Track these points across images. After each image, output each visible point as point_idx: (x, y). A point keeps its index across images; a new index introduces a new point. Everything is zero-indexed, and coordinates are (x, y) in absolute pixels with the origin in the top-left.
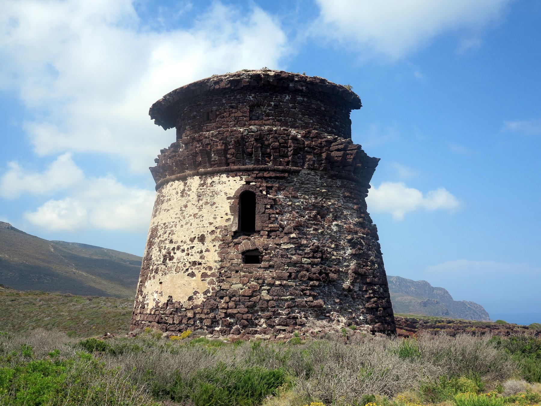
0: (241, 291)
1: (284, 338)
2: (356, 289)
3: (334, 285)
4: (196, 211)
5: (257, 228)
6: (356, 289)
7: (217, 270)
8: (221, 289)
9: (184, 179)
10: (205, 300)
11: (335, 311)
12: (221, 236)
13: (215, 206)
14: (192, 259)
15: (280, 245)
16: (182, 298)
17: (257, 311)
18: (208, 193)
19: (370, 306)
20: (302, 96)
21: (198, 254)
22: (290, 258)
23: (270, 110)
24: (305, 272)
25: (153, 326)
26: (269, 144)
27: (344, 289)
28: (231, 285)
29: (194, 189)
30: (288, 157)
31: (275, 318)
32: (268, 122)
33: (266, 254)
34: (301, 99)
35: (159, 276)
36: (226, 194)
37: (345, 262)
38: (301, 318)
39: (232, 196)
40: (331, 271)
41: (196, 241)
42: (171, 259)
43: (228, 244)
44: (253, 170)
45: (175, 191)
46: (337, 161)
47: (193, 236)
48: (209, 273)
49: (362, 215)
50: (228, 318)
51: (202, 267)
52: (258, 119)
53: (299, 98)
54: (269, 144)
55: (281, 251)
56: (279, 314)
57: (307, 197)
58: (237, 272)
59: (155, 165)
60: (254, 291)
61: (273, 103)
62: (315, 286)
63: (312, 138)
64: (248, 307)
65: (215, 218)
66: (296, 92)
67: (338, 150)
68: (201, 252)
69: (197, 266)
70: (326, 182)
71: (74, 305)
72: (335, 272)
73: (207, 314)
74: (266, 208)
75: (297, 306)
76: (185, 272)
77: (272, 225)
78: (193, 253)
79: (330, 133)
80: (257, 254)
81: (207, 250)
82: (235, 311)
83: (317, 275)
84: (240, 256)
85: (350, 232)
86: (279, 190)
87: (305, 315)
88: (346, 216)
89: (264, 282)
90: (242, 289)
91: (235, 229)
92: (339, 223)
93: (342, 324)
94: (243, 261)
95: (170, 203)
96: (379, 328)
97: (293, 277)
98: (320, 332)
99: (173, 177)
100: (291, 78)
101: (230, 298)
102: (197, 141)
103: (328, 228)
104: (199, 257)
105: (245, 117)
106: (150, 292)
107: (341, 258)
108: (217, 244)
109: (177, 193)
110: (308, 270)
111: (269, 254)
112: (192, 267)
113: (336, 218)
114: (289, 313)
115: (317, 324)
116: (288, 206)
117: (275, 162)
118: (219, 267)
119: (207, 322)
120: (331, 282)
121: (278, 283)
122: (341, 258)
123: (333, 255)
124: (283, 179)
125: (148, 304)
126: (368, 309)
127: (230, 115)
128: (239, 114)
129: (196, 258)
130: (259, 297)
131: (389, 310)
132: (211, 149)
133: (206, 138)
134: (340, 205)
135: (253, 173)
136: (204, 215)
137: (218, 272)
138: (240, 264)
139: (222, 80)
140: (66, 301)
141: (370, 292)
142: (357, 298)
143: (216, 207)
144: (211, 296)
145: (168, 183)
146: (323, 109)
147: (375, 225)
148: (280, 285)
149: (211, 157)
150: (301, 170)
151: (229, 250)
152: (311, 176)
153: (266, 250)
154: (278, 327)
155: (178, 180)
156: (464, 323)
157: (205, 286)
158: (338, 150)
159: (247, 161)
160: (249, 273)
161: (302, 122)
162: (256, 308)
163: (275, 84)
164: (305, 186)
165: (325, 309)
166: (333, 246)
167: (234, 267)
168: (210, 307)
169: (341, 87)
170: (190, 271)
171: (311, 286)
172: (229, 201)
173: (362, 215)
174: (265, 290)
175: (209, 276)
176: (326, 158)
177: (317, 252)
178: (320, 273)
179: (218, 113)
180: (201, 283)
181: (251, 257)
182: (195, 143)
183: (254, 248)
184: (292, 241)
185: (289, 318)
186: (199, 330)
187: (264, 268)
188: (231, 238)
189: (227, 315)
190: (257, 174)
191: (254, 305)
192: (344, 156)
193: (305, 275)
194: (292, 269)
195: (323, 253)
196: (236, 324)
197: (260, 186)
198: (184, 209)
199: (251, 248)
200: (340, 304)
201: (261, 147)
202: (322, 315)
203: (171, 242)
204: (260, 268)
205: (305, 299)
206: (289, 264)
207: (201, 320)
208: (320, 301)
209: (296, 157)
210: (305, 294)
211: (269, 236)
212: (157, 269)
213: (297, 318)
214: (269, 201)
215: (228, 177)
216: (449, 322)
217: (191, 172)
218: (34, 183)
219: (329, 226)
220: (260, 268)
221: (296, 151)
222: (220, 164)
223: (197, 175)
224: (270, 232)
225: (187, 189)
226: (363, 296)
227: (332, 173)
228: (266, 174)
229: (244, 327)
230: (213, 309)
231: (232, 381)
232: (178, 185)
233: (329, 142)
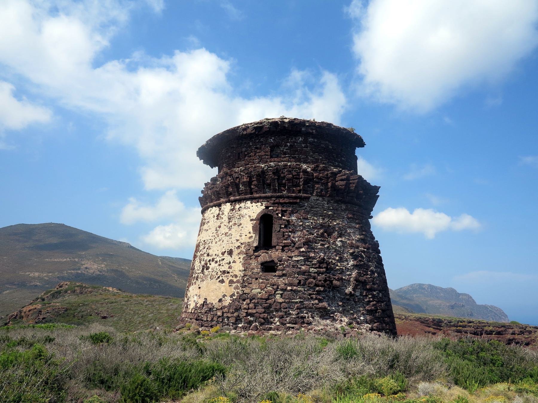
0: (259, 295)
1: (292, 334)
2: (358, 294)
3: (338, 291)
4: (227, 230)
5: (273, 244)
6: (358, 294)
8: (243, 293)
9: (219, 205)
11: (338, 312)
13: (241, 226)
14: (223, 269)
15: (292, 257)
17: (272, 312)
19: (369, 309)
20: (312, 138)
22: (300, 268)
23: (286, 149)
24: (312, 280)
25: (192, 323)
26: (285, 177)
27: (346, 294)
29: (226, 213)
30: (300, 186)
31: (287, 317)
32: (285, 159)
33: (280, 265)
35: (198, 282)
36: (250, 216)
37: (348, 271)
38: (308, 317)
39: (254, 218)
40: (335, 278)
41: (226, 254)
42: (208, 268)
43: (251, 256)
45: (212, 215)
46: (341, 189)
47: (224, 251)
48: (235, 280)
49: (364, 233)
52: (277, 157)
53: (311, 140)
54: (285, 177)
56: (290, 314)
57: (316, 218)
58: (257, 279)
59: (202, 195)
60: (270, 295)
61: (289, 144)
62: (320, 291)
63: (320, 171)
64: (264, 308)
65: (241, 236)
66: (307, 135)
67: (342, 180)
68: (230, 263)
69: (226, 275)
70: (332, 206)
71: (171, 305)
72: (338, 280)
73: (233, 313)
74: (281, 228)
75: (305, 308)
76: (217, 279)
77: (286, 242)
79: (336, 167)
80: (273, 265)
81: (234, 262)
82: (254, 311)
84: (260, 266)
85: (352, 246)
86: (292, 213)
87: (311, 315)
88: (349, 233)
89: (278, 288)
90: (260, 293)
91: (256, 244)
92: (343, 239)
93: (344, 324)
94: (263, 270)
95: (209, 224)
96: (377, 327)
97: (302, 283)
98: (322, 329)
99: (212, 204)
101: (251, 300)
102: (230, 175)
103: (333, 244)
105: (267, 155)
106: (192, 295)
107: (344, 268)
108: (242, 256)
109: (214, 216)
110: (314, 278)
111: (283, 264)
113: (340, 235)
114: (298, 314)
115: (322, 323)
116: (301, 226)
117: (289, 190)
118: (242, 275)
119: (232, 320)
120: (335, 288)
121: (289, 288)
122: (344, 268)
123: (337, 266)
124: (295, 204)
125: (190, 305)
126: (368, 311)
127: (255, 155)
128: (262, 153)
129: (226, 268)
130: (273, 300)
131: (388, 312)
132: (239, 182)
133: (236, 173)
134: (344, 224)
136: (233, 233)
139: (248, 127)
140: (166, 302)
141: (370, 296)
142: (358, 301)
145: (208, 209)
146: (331, 147)
147: (377, 241)
148: (291, 290)
149: (240, 188)
150: (310, 197)
151: (251, 262)
153: (280, 261)
154: (288, 325)
155: (215, 206)
156: (483, 323)
157: (232, 290)
158: (342, 180)
159: (267, 190)
160: (267, 280)
162: (271, 309)
163: (290, 129)
164: (315, 209)
166: (337, 258)
168: (234, 307)
169: (344, 129)
170: (221, 278)
171: (317, 291)
173: (364, 233)
174: (279, 294)
175: (235, 283)
176: (331, 187)
177: (323, 263)
178: (325, 280)
179: (246, 153)
180: (229, 288)
181: (269, 267)
182: (228, 177)
183: (271, 259)
184: (302, 254)
185: (298, 317)
186: (226, 326)
187: (278, 276)
189: (248, 314)
191: (270, 306)
192: (347, 185)
193: (312, 282)
194: (301, 277)
195: (328, 264)
196: (256, 322)
197: (276, 211)
198: (218, 229)
199: (268, 259)
200: (343, 306)
201: (278, 179)
203: (208, 255)
204: (275, 276)
205: (312, 302)
207: (228, 318)
208: (325, 304)
209: (306, 186)
210: (312, 298)
211: (283, 250)
212: (198, 277)
213: (305, 317)
214: (284, 222)
215: (252, 203)
216: (470, 322)
217: (224, 200)
218: (146, 213)
219: (334, 242)
220: (275, 276)
221: (306, 182)
222: (246, 194)
223: (229, 202)
224: (283, 247)
225: (221, 213)
226: (364, 300)
227: (337, 198)
228: (281, 201)
229: (262, 324)
230: (237, 309)
231: (165, 374)
232: (215, 210)
233: (334, 174)
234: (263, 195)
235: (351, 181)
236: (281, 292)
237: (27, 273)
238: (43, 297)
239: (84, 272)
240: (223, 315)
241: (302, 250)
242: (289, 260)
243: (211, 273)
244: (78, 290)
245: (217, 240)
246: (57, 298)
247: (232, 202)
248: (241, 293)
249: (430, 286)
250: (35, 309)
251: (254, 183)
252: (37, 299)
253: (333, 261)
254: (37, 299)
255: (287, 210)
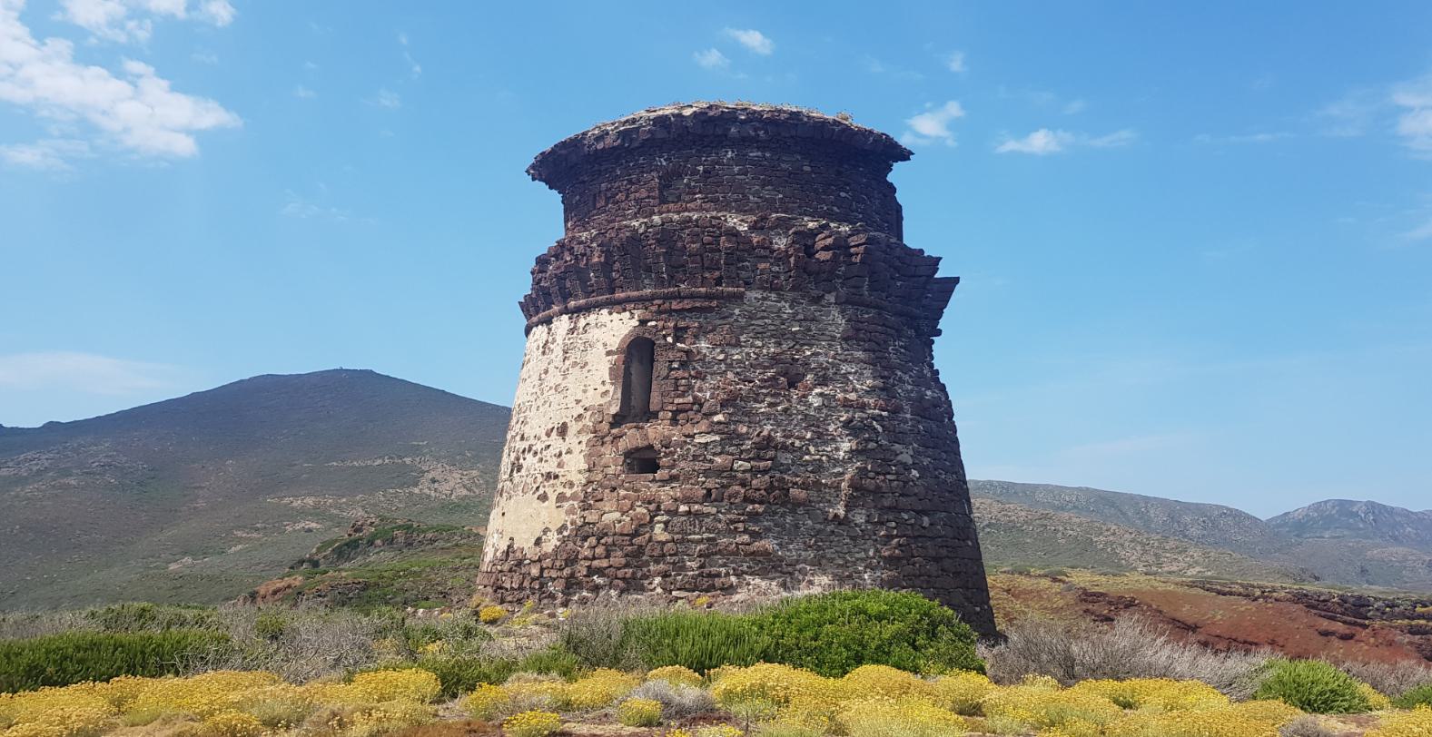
2: (860, 519)
6: (860, 519)
7: (580, 488)
10: (558, 544)
12: (591, 424)
13: (587, 368)
14: (546, 468)
15: (693, 437)
16: (527, 540)
17: (647, 564)
18: (578, 345)
20: (758, 149)
21: (554, 459)
22: (711, 461)
24: (737, 488)
28: (602, 515)
29: (559, 340)
33: (666, 455)
34: (759, 154)
37: (835, 466)
39: (614, 349)
42: (519, 468)
43: (603, 438)
44: (652, 298)
45: (535, 345)
47: (550, 426)
48: (568, 493)
50: (595, 578)
51: (559, 483)
55: (693, 449)
58: (614, 489)
60: (641, 526)
61: (701, 168)
62: (757, 513)
65: (585, 391)
68: (560, 454)
72: (805, 486)
76: (534, 493)
77: (681, 400)
78: (548, 458)
80: (652, 455)
81: (569, 452)
82: (604, 563)
83: (762, 492)
86: (701, 333)
88: (845, 376)
89: (658, 508)
91: (614, 409)
92: (826, 390)
97: (713, 496)
100: (730, 117)
101: (598, 540)
104: (556, 464)
107: (824, 458)
108: (584, 438)
110: (743, 485)
111: (673, 453)
112: (546, 484)
113: (823, 381)
116: (722, 359)
118: (584, 481)
121: (683, 508)
123: (808, 453)
124: (710, 309)
127: (627, 197)
129: (551, 466)
130: (647, 536)
133: (581, 243)
135: (653, 305)
137: (582, 491)
138: (619, 475)
143: (589, 371)
144: (568, 537)
148: (689, 513)
151: (602, 449)
152: (769, 303)
160: (636, 491)
161: (759, 200)
165: (781, 559)
167: (609, 480)
168: (565, 556)
170: (541, 491)
171: (749, 514)
172: (610, 358)
174: (659, 522)
177: (767, 447)
181: (643, 461)
183: (646, 443)
184: (716, 428)
188: (607, 427)
189: (591, 571)
190: (659, 306)
191: (640, 550)
193: (738, 493)
194: (711, 483)
197: (664, 328)
198: (543, 376)
199: (641, 443)
202: (776, 571)
204: (654, 480)
206: (706, 473)
208: (768, 544)
211: (674, 421)
215: (610, 313)
223: (566, 314)
228: (675, 305)
230: (572, 560)
234: (636, 293)
235: (852, 250)
236: (665, 518)
237: (286, 500)
238: (316, 558)
239: (427, 491)
240: (541, 575)
241: (719, 418)
242: (685, 442)
243: (524, 479)
244: (400, 536)
245: (540, 403)
246: (349, 559)
247: (573, 313)
248: (579, 522)
249: (1372, 507)
250: (289, 587)
251: (617, 266)
252: (302, 562)
253: (797, 443)
254: (302, 562)
255: (688, 328)
